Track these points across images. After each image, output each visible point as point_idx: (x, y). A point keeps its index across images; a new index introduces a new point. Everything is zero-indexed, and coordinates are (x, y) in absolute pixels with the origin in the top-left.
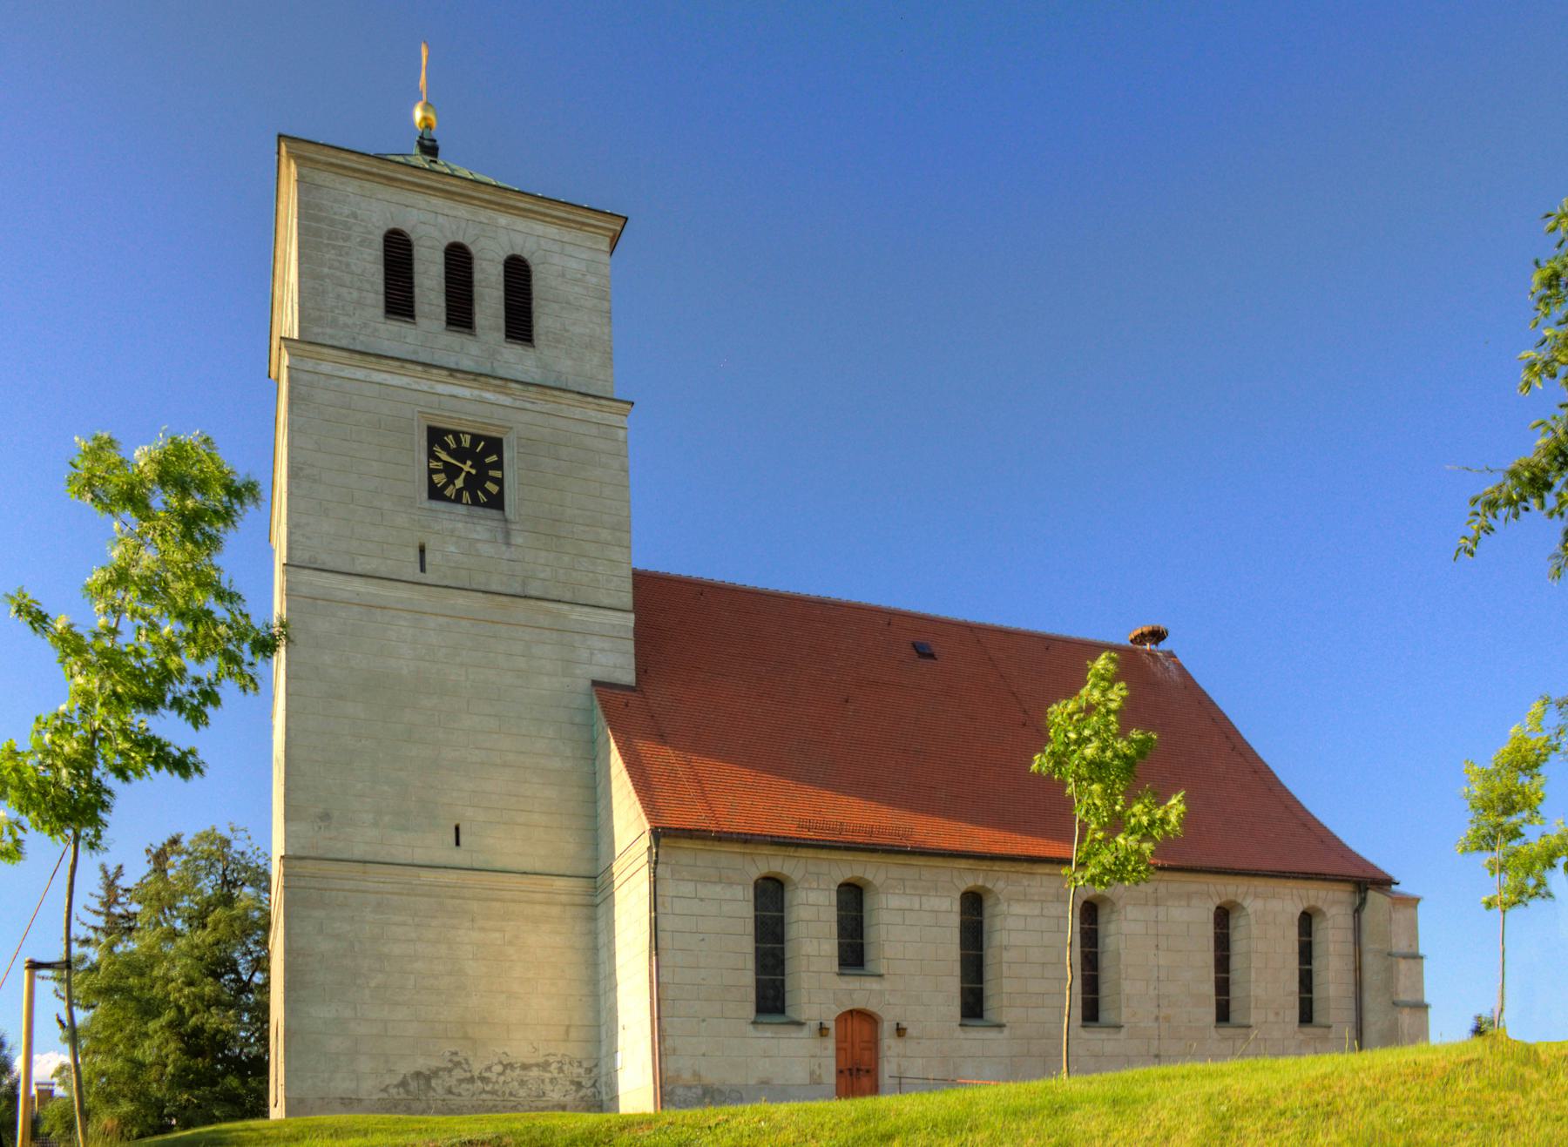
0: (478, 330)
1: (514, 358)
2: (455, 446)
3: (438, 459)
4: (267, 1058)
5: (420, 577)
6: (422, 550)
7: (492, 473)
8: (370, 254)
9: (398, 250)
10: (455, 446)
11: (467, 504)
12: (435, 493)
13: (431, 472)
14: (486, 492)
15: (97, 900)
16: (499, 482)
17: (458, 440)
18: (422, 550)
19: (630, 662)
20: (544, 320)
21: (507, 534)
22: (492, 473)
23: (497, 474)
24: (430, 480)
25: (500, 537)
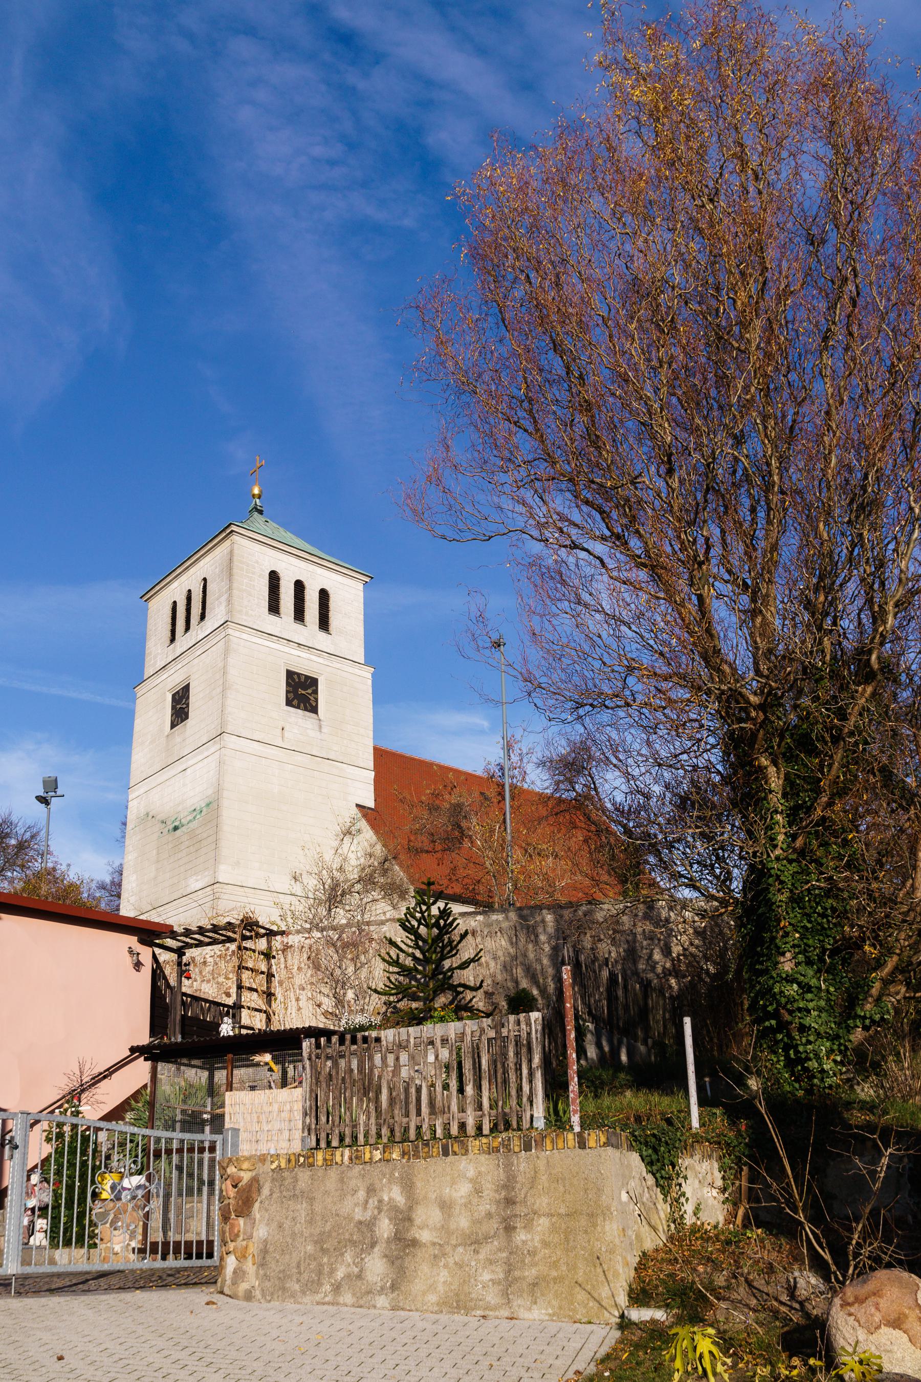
9: (274, 579)
12: (289, 703)
21: (320, 727)
25: (317, 728)
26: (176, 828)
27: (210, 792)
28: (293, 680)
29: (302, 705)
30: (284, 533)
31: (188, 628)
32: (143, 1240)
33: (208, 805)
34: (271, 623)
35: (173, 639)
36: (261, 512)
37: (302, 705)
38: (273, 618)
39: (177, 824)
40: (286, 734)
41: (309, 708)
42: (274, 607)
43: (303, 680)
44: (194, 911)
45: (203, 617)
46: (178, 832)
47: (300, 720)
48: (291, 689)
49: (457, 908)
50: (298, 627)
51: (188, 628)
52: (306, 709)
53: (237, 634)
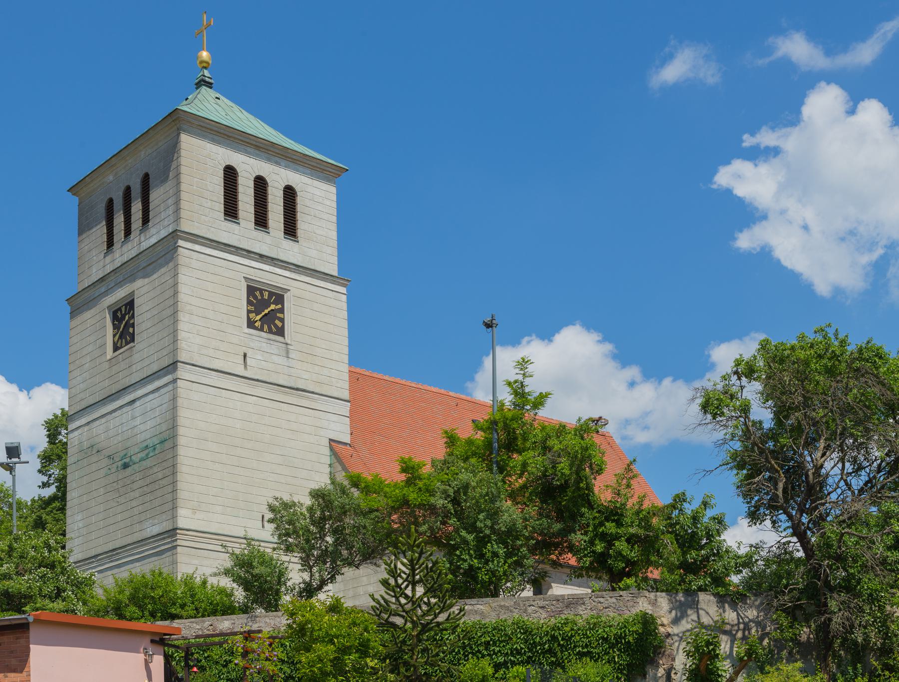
0: (241, 221)
1: (288, 251)
2: (267, 298)
3: (770, 463)
4: (697, 599)
5: (240, 370)
6: (245, 356)
7: (278, 315)
8: (217, 180)
10: (267, 298)
11: (266, 332)
12: (251, 324)
13: (249, 312)
14: (276, 326)
15: (300, 565)
16: (282, 320)
17: (262, 295)
18: (245, 356)
19: (348, 430)
20: (302, 225)
21: (287, 352)
22: (278, 315)
23: (250, 308)
24: (248, 317)
25: (284, 353)
26: (126, 466)
27: (164, 427)
28: (255, 297)
29: (266, 327)
30: (239, 114)
31: (128, 232)
32: (224, 633)
33: (162, 442)
34: (227, 232)
35: (110, 243)
36: (209, 85)
37: (266, 327)
38: (230, 225)
39: (127, 460)
40: (248, 360)
41: (274, 329)
42: (231, 211)
43: (266, 297)
44: (237, 545)
45: (146, 220)
46: (129, 471)
47: (264, 344)
48: (252, 308)
49: (575, 564)
50: (260, 234)
51: (128, 232)
52: (270, 331)
53: (189, 245)
